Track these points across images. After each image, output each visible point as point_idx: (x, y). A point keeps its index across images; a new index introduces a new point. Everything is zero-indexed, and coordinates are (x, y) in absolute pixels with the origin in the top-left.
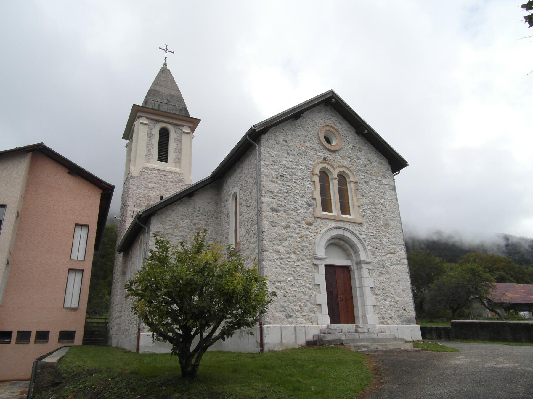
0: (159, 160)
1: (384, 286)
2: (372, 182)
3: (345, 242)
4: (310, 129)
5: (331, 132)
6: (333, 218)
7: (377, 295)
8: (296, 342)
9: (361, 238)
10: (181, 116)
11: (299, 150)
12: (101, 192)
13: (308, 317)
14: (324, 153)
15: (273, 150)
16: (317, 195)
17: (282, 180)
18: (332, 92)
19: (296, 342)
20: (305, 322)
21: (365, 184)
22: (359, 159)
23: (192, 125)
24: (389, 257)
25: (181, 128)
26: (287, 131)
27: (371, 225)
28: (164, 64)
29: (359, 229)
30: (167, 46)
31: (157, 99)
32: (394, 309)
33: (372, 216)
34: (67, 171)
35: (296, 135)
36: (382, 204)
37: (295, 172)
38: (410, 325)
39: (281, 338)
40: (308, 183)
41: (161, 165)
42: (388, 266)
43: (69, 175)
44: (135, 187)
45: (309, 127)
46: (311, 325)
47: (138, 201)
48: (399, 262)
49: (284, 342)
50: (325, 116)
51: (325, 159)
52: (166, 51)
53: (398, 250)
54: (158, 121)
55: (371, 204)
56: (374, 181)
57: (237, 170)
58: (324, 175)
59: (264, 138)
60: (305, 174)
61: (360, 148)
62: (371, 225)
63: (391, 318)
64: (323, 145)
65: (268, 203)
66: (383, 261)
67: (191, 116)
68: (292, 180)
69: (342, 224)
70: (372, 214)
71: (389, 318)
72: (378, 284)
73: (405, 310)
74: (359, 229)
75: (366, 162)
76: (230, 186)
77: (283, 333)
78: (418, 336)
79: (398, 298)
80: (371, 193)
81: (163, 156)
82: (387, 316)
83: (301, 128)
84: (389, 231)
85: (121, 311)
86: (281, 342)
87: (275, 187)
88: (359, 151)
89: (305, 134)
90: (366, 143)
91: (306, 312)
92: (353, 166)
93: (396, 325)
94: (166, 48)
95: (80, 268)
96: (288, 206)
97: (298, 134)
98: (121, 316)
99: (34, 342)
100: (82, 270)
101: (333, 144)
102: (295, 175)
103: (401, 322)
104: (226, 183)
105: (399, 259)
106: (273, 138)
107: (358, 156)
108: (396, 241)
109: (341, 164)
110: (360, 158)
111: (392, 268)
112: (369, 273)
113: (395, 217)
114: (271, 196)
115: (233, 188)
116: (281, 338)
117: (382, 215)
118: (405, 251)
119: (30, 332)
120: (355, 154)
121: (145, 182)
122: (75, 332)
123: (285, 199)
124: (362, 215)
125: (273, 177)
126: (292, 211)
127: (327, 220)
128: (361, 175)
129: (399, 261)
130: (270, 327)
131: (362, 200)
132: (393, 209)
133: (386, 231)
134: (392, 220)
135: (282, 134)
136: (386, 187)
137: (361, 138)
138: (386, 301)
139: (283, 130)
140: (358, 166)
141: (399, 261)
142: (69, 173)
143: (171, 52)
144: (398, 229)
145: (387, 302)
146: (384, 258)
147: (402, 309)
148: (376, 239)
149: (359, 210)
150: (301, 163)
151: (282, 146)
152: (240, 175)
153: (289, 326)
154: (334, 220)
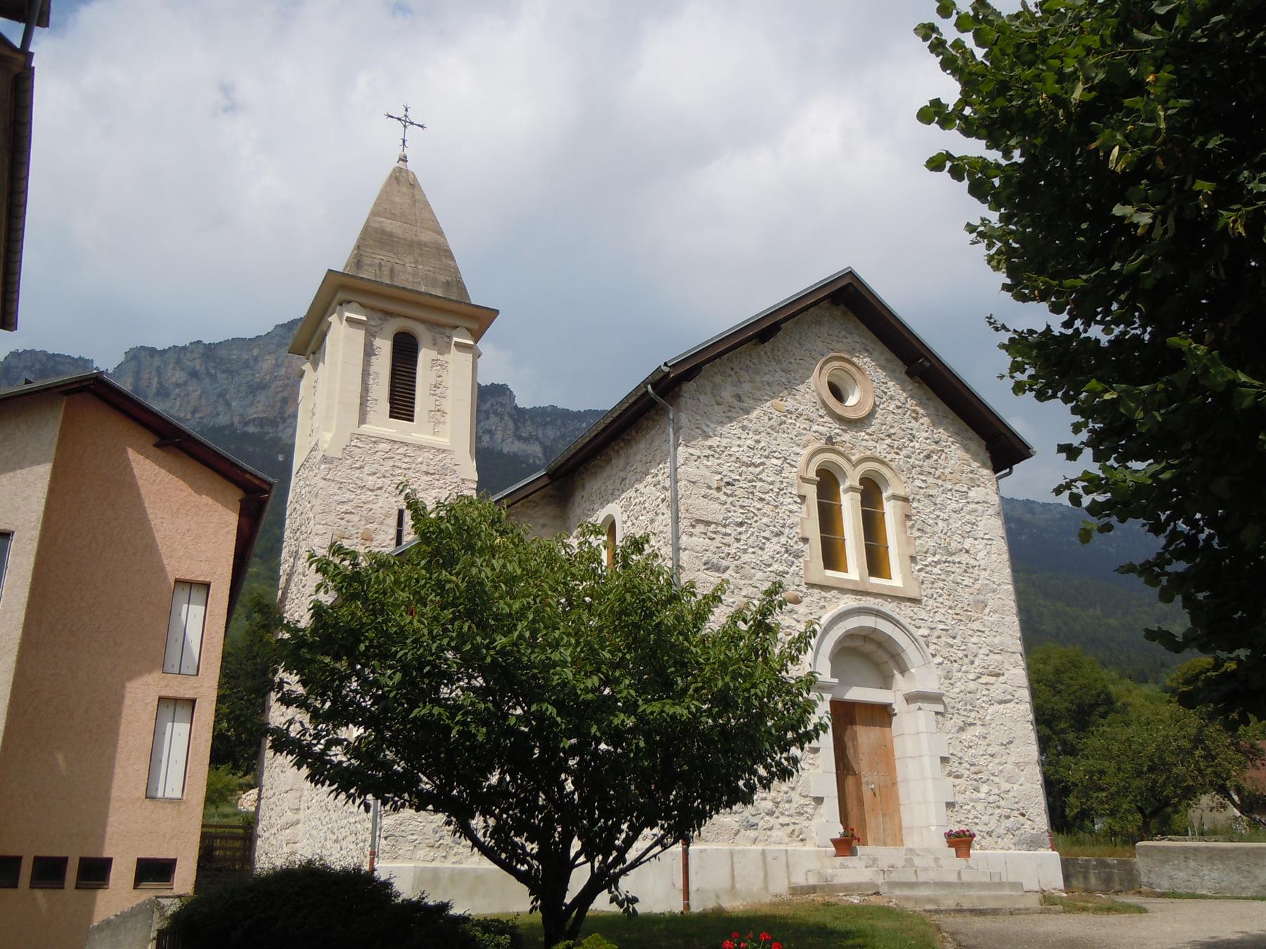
0: (393, 415)
1: (974, 756)
2: (944, 495)
3: (879, 645)
4: (795, 366)
5: (846, 371)
6: (851, 587)
7: (957, 777)
8: (766, 888)
9: (917, 637)
10: (450, 300)
11: (770, 419)
12: (240, 498)
13: (792, 827)
14: (830, 425)
15: (710, 419)
16: (813, 530)
17: (729, 492)
18: (851, 274)
19: (687, 906)
20: (786, 839)
21: (926, 501)
22: (913, 438)
23: (475, 326)
24: (986, 684)
25: (448, 332)
26: (742, 373)
27: (942, 603)
28: (400, 159)
29: (912, 614)
30: (406, 110)
31: (386, 254)
32: (997, 811)
33: (944, 580)
34: (155, 439)
35: (762, 382)
36: (967, 552)
37: (760, 473)
38: (1037, 852)
39: (733, 877)
40: (790, 500)
41: (397, 429)
42: (983, 705)
43: (158, 451)
44: (333, 485)
45: (792, 361)
46: (799, 847)
47: (343, 523)
48: (1009, 697)
49: (738, 886)
50: (830, 332)
51: (830, 439)
52: (406, 122)
53: (1006, 666)
54: (389, 314)
55: (941, 551)
56: (949, 493)
57: (614, 461)
58: (827, 482)
59: (689, 387)
60: (784, 478)
61: (914, 411)
62: (942, 603)
63: (990, 834)
64: (825, 406)
65: (698, 549)
66: (970, 693)
67: (474, 302)
68: (752, 493)
69: (870, 602)
70: (943, 577)
71: (984, 834)
72: (958, 749)
73: (1023, 815)
74: (912, 614)
75: (929, 447)
76: (595, 498)
77: (735, 866)
78: (1054, 880)
79: (1006, 786)
80: (941, 524)
81: (402, 405)
82: (980, 828)
83: (774, 364)
84: (986, 618)
85: (298, 809)
86: (733, 887)
87: (713, 510)
88: (914, 418)
89: (784, 380)
90: (929, 399)
91: (788, 816)
92: (897, 457)
93: (1002, 852)
94: (406, 116)
95: (187, 696)
96: (745, 558)
97: (767, 378)
98: (298, 822)
99: (74, 885)
100: (193, 702)
101: (852, 400)
102: (761, 480)
103: (1014, 844)
104: (584, 488)
105: (1010, 689)
106: (708, 390)
107: (910, 432)
108: (1002, 644)
109: (868, 453)
110: (914, 437)
111: (992, 709)
112: (937, 722)
113: (999, 585)
114: (705, 534)
115: (602, 504)
116: (733, 877)
117: (967, 578)
118: (1023, 669)
119: (18, 860)
120: (903, 426)
121: (357, 473)
122: (175, 861)
123: (738, 540)
124: (921, 578)
125: (710, 487)
126: (753, 568)
127: (834, 593)
128: (918, 478)
129: (1010, 693)
130: (705, 850)
131: (918, 542)
132: (996, 564)
133: (978, 619)
134: (994, 591)
135: (730, 379)
136: (979, 507)
137: (917, 385)
138: (979, 792)
139: (732, 369)
140: (910, 457)
141: (1010, 693)
142: (157, 446)
143: (419, 126)
144: (1007, 613)
145: (982, 795)
146: (972, 686)
147: (1016, 813)
148: (954, 638)
149: (913, 565)
150: (775, 452)
151: (728, 408)
152: (622, 474)
153: (749, 850)
154: (853, 590)
